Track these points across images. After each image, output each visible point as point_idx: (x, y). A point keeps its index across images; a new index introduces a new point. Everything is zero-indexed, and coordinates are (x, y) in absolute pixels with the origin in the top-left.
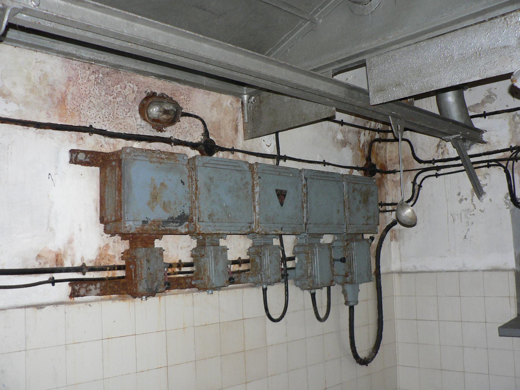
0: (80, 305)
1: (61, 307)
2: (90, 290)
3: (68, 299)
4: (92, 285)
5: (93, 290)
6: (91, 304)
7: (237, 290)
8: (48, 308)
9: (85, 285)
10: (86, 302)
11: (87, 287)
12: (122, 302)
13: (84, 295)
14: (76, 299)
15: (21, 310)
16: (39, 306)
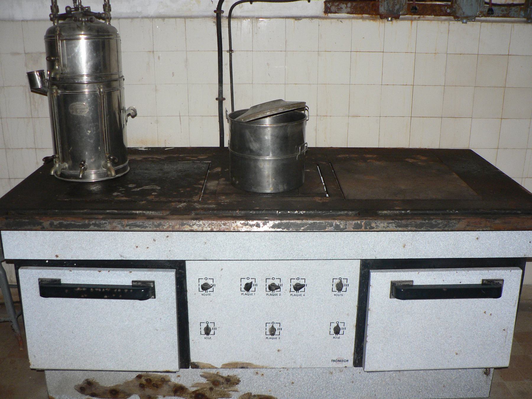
0: (332, 20)
1: (316, 21)
2: (342, 8)
3: (322, 14)
4: (343, 4)
5: (344, 8)
6: (343, 20)
7: (506, 24)
8: (304, 20)
9: (336, 4)
10: (338, 18)
11: (338, 5)
12: (372, 22)
13: (335, 13)
14: (330, 15)
15: (282, 19)
16: (297, 18)
